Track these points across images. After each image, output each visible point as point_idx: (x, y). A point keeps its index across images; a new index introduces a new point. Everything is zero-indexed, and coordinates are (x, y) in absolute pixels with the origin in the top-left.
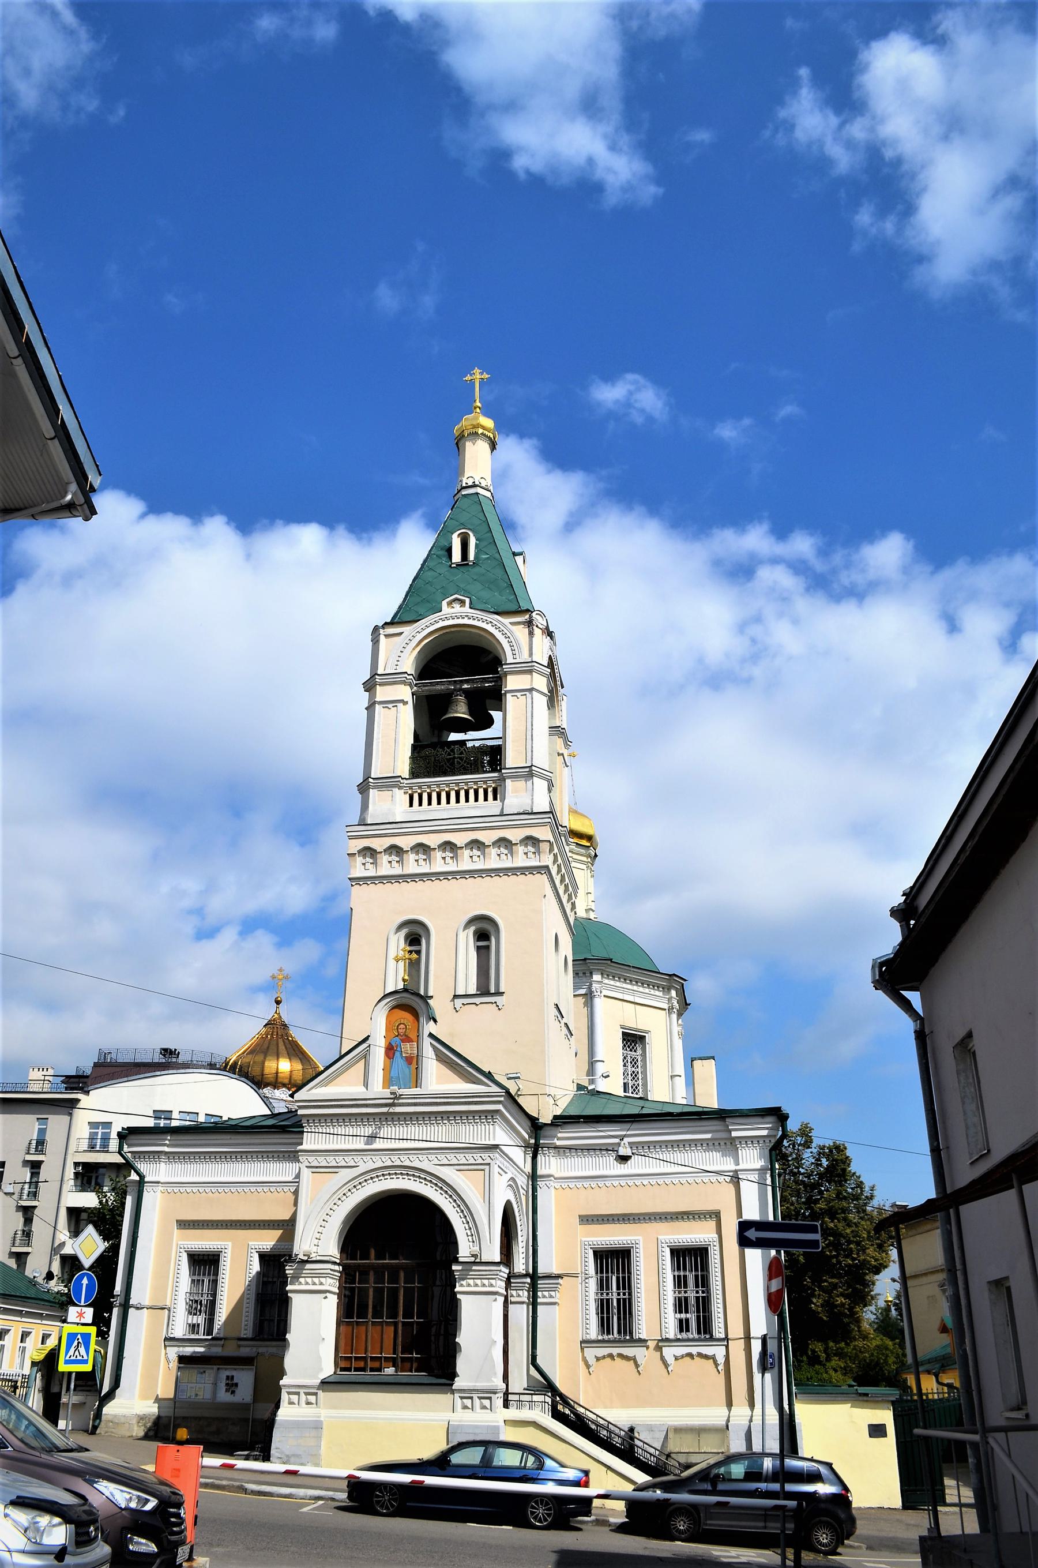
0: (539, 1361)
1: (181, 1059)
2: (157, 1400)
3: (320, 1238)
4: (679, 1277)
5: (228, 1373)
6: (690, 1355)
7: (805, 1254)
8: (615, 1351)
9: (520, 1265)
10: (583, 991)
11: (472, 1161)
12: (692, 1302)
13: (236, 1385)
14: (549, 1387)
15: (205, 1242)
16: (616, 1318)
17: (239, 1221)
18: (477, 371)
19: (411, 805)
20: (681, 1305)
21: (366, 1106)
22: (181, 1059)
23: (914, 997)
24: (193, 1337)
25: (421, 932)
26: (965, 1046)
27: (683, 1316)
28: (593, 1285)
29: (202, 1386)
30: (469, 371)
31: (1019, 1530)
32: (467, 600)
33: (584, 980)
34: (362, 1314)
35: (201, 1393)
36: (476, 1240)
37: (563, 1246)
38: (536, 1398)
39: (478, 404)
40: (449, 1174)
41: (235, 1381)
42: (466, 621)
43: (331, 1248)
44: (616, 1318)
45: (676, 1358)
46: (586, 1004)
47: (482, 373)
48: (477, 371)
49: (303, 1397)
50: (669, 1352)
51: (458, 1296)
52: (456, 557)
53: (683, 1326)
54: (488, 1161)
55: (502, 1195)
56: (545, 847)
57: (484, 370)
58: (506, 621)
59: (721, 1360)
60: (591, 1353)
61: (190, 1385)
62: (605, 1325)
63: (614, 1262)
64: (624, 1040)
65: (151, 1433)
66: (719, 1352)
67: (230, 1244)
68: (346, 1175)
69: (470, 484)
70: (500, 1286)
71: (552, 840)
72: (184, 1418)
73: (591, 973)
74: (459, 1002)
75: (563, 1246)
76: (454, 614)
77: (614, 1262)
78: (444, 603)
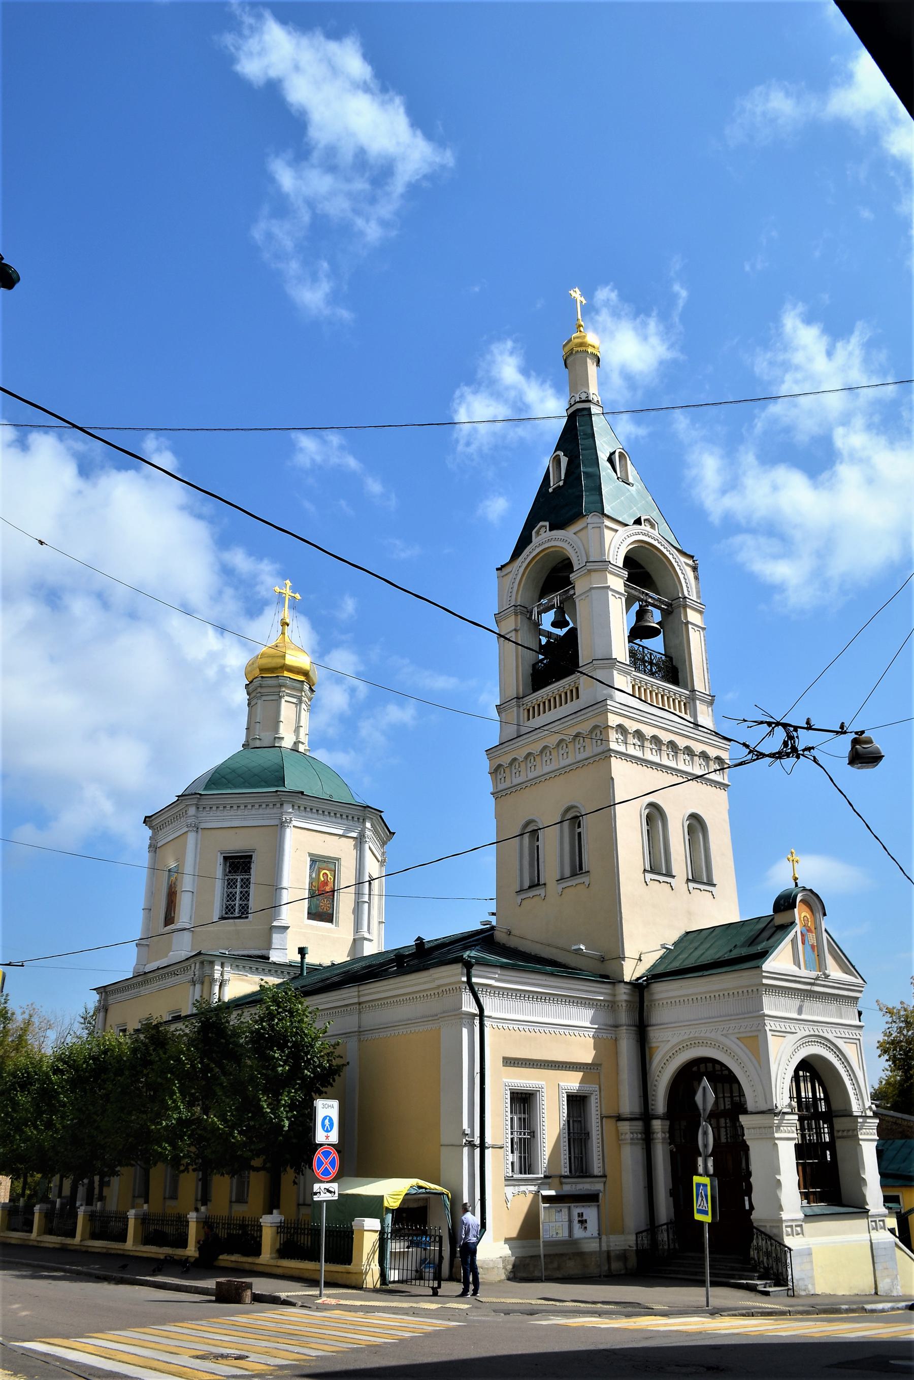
2: (507, 1240)
4: (524, 1119)
5: (579, 1210)
10: (354, 835)
11: (779, 1029)
13: (586, 1221)
15: (525, 1080)
17: (557, 1062)
21: (799, 982)
29: (558, 1224)
33: (357, 824)
35: (560, 1232)
40: (840, 1043)
41: (584, 1218)
42: (655, 543)
46: (355, 847)
51: (861, 1142)
54: (858, 1037)
58: (683, 559)
61: (551, 1224)
65: (512, 1275)
69: (584, 398)
72: (532, 1257)
73: (282, 805)
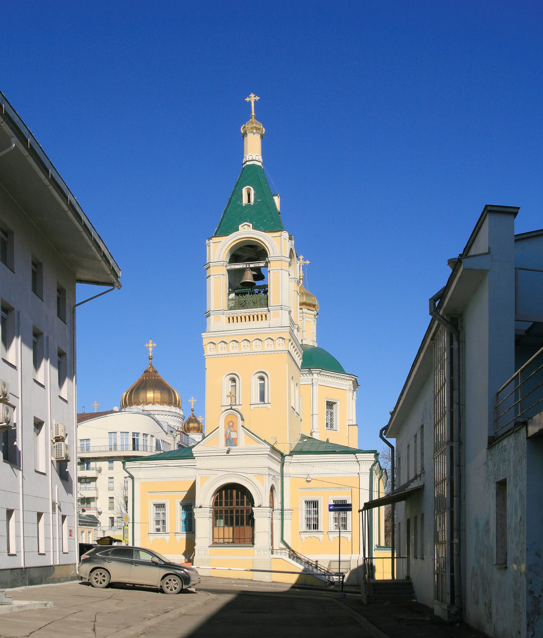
0: (284, 539)
3: (205, 499)
7: (88, 555)
8: (312, 535)
16: (313, 525)
18: (252, 95)
23: (393, 441)
30: (248, 95)
31: (374, 557)
32: (251, 225)
34: (242, 524)
36: (260, 497)
39: (253, 114)
45: (334, 538)
47: (255, 97)
48: (252, 95)
49: (203, 552)
56: (287, 341)
57: (256, 94)
59: (350, 538)
60: (303, 536)
64: (327, 404)
67: (168, 501)
74: (252, 407)
75: (294, 500)
76: (246, 232)
78: (240, 226)
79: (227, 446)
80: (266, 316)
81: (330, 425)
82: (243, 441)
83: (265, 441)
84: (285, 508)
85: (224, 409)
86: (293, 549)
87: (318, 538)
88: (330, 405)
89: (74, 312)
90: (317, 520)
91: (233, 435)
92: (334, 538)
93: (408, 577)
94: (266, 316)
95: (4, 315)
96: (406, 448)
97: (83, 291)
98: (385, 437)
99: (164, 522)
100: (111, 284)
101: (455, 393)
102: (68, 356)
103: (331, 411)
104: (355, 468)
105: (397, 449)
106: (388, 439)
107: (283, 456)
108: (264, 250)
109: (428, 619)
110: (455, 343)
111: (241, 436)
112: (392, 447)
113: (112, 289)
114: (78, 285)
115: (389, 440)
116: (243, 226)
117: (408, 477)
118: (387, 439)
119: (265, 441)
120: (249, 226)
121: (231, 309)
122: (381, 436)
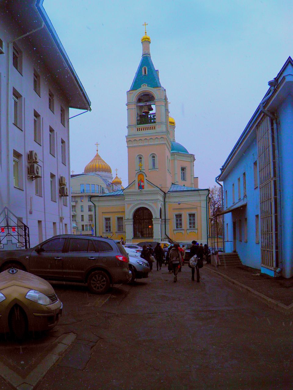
0: (166, 234)
1: (207, 244)
3: (129, 215)
6: (192, 232)
8: (179, 232)
9: (163, 217)
12: (192, 224)
14: (168, 238)
15: (107, 216)
16: (179, 224)
19: (138, 131)
20: (190, 224)
22: (207, 244)
23: (222, 183)
24: (177, 229)
25: (141, 156)
26: (226, 191)
27: (190, 225)
28: (175, 220)
32: (147, 85)
36: (156, 214)
37: (171, 215)
38: (166, 240)
43: (131, 216)
44: (179, 224)
50: (188, 231)
52: (143, 73)
53: (190, 227)
55: (160, 206)
60: (175, 232)
62: (177, 227)
63: (179, 216)
66: (196, 231)
68: (132, 205)
70: (160, 222)
71: (166, 137)
74: (150, 171)
75: (171, 215)
76: (145, 88)
77: (179, 216)
78: (142, 85)
79: (139, 189)
80: (155, 127)
81: (184, 178)
82: (147, 188)
83: (157, 186)
84: (166, 218)
85: (136, 172)
86: (171, 238)
87: (182, 233)
88: (183, 169)
89: (68, 121)
90: (194, 223)
91: (142, 184)
92: (189, 232)
93: (235, 252)
94: (155, 127)
95: (36, 119)
96: (232, 186)
97: (72, 111)
98: (218, 181)
99: (110, 227)
100: (86, 109)
101: (276, 152)
102: (66, 143)
103: (183, 171)
104: (198, 198)
105: (224, 187)
106: (219, 182)
107: (165, 193)
108: (153, 96)
109: (259, 274)
110: (275, 125)
111: (145, 184)
112: (222, 186)
113: (87, 111)
114: (70, 109)
115: (220, 182)
116: (143, 85)
117: (234, 199)
118: (219, 182)
119: (157, 186)
120: (146, 85)
121: (138, 124)
122: (216, 181)
